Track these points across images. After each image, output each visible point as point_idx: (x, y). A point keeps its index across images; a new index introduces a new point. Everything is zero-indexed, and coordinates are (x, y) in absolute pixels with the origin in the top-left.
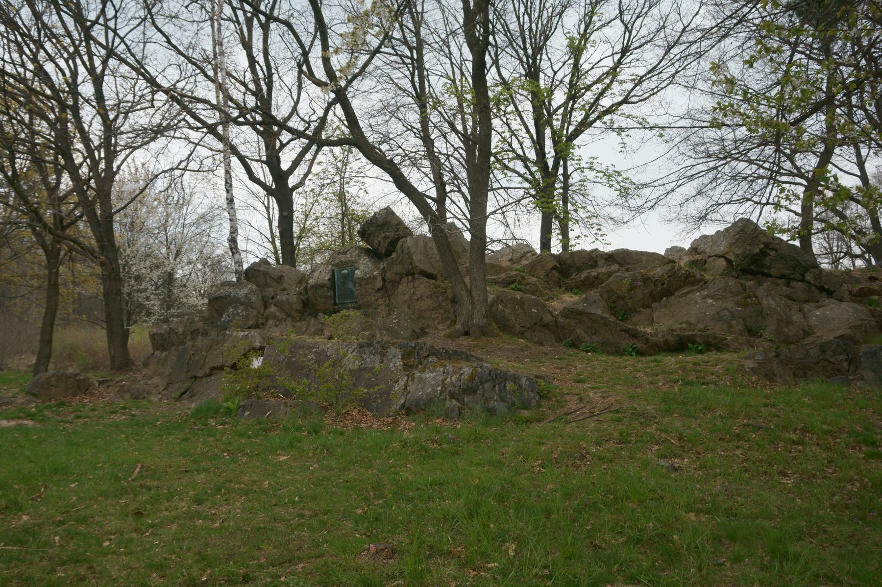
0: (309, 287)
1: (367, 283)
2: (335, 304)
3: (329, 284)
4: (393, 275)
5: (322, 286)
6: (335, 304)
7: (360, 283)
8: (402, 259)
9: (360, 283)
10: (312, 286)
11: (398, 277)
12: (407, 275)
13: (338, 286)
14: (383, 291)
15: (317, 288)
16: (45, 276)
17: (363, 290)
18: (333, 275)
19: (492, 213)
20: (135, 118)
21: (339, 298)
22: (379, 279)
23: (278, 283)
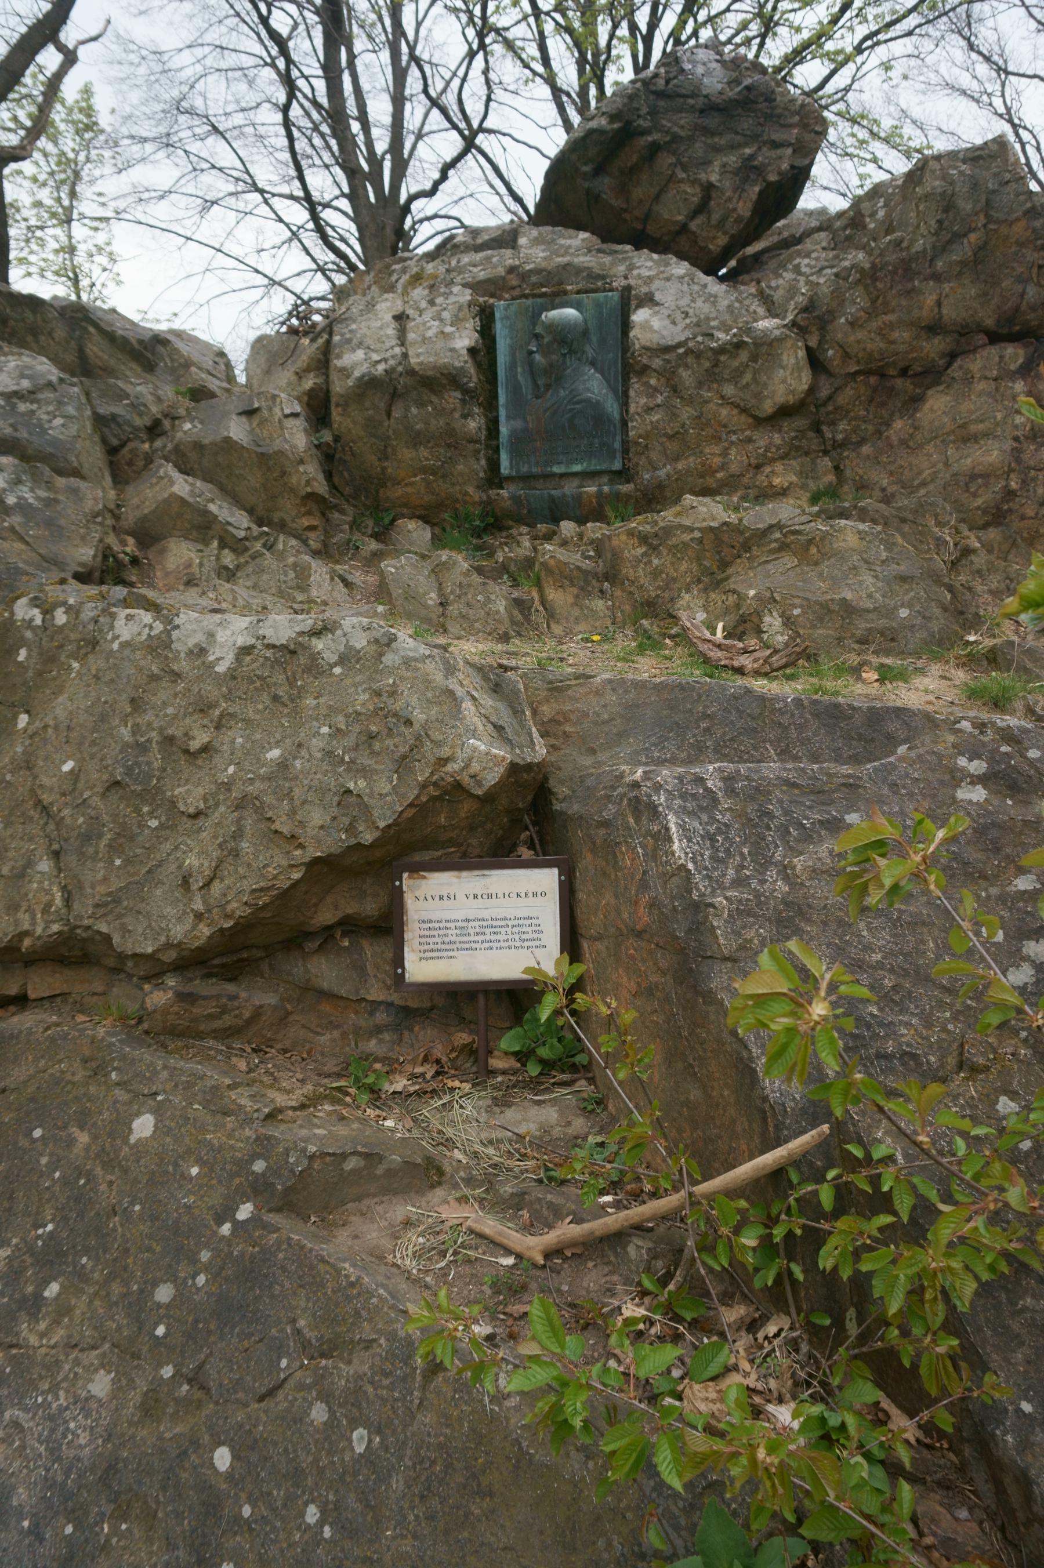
0: (339, 387)
1: (712, 377)
2: (494, 478)
3: (473, 378)
4: (902, 335)
5: (451, 379)
6: (494, 478)
7: (669, 376)
8: (981, 248)
9: (669, 376)
10: (370, 384)
11: (933, 347)
12: (994, 338)
13: (515, 389)
14: (801, 422)
15: (395, 395)
16: (758, 396)
17: (686, 413)
18: (486, 331)
19: (819, 201)
20: (434, 671)
21: (516, 452)
22: (794, 356)
23: (869, 1548)
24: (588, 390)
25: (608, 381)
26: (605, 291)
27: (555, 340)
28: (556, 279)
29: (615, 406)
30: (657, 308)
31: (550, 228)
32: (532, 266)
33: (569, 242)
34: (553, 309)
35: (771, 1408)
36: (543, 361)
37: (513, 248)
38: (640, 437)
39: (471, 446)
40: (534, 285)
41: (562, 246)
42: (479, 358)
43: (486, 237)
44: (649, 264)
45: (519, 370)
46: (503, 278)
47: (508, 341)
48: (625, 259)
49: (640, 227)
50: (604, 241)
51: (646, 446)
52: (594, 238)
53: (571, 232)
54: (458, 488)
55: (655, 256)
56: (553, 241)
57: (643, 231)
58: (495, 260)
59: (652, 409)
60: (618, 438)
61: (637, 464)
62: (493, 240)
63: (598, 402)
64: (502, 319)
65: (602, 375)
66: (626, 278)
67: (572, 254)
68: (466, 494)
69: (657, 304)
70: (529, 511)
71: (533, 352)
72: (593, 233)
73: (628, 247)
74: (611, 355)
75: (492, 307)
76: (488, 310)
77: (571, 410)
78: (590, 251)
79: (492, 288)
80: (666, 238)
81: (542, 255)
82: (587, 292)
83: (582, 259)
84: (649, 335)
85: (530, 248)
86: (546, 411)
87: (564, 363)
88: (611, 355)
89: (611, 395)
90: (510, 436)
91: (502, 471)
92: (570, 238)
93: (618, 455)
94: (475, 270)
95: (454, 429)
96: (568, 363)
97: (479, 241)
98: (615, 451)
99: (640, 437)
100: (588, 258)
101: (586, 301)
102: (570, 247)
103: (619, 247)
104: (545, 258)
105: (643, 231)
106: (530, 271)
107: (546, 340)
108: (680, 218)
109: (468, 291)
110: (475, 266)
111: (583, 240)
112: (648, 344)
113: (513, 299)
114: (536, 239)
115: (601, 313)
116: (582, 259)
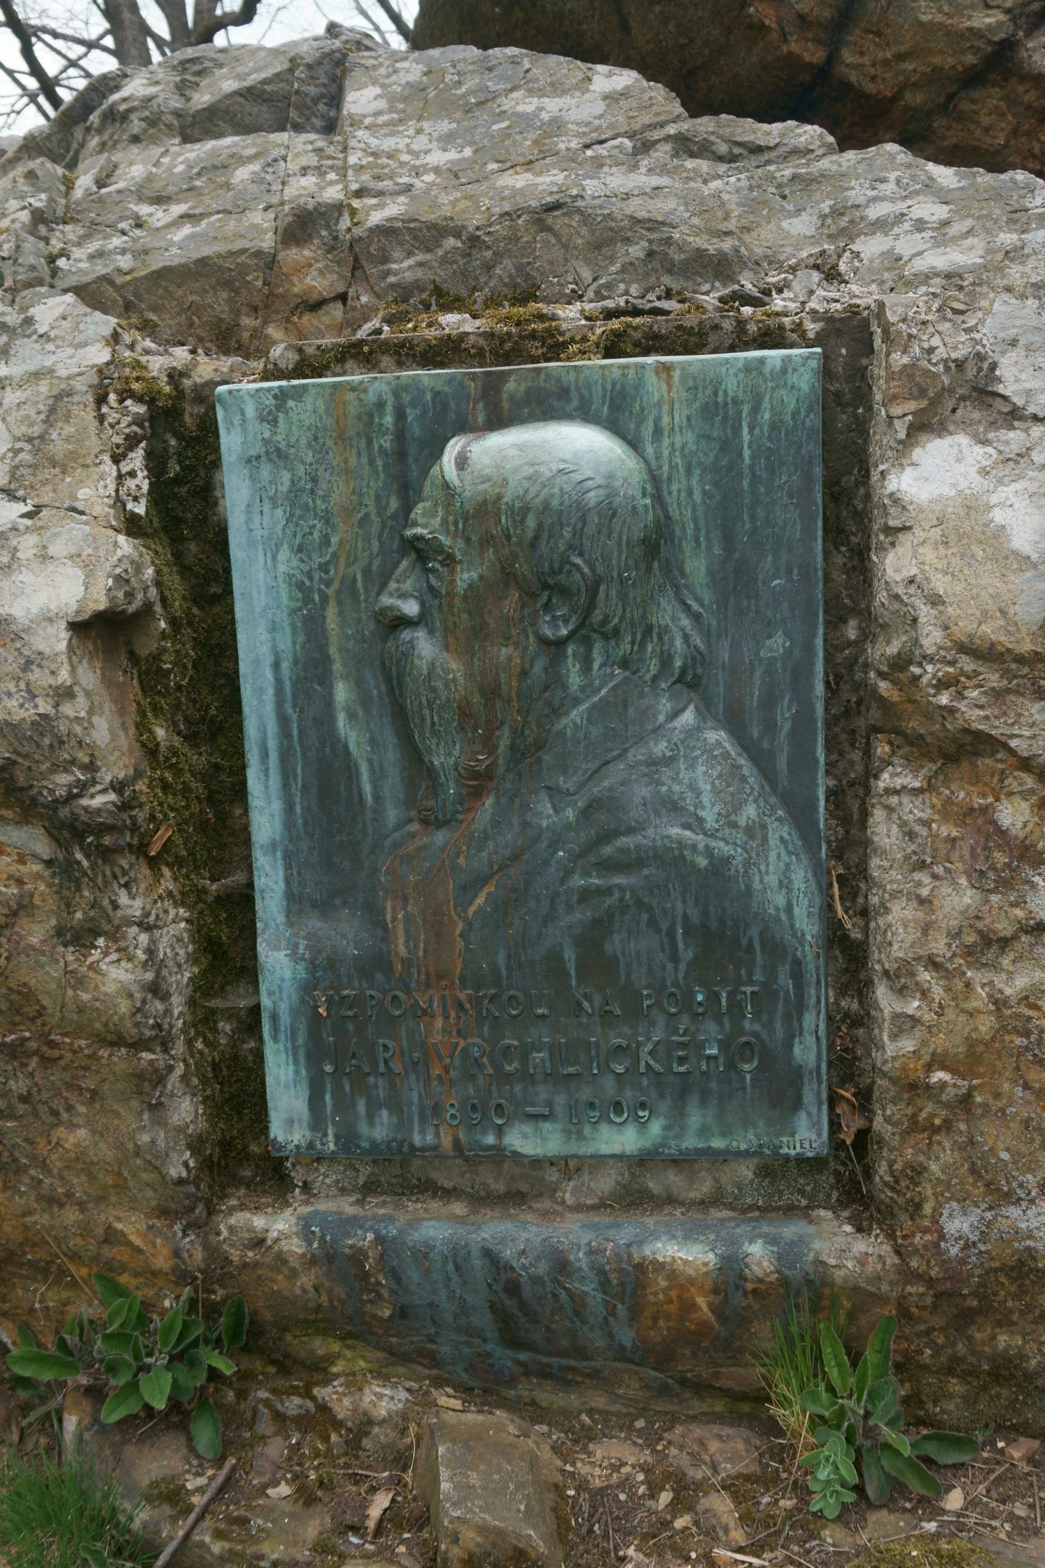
24: (673, 807)
25: (762, 761)
26: (741, 341)
27: (507, 576)
28: (504, 269)
29: (801, 877)
30: (1014, 438)
31: (472, 52)
32: (394, 209)
33: (552, 105)
34: (497, 422)
35: (516, 452)
36: (455, 667)
37: (330, 128)
38: (938, 1061)
39: (118, 1059)
40: (404, 292)
41: (524, 121)
42: (146, 647)
43: (229, 85)
44: (931, 210)
45: (342, 693)
46: (269, 262)
47: (286, 561)
48: (805, 183)
49: (814, 55)
50: (696, 107)
51: (965, 1101)
52: (658, 92)
53: (558, 64)
54: (71, 1216)
55: (945, 175)
56: (487, 99)
57: (824, 72)
58: (242, 174)
59: (1005, 943)
60: (814, 1021)
61: (917, 1172)
62: (249, 94)
63: (719, 865)
64: (252, 461)
65: (736, 728)
66: (832, 276)
67: (571, 159)
68: (111, 1237)
69: (1014, 415)
70: (402, 1313)
71: (401, 622)
72: (649, 72)
73: (809, 134)
74: (777, 644)
75: (204, 396)
76: (191, 413)
77: (586, 895)
78: (646, 147)
79: (220, 304)
80: (915, 98)
81: (438, 157)
82: (652, 344)
83: (617, 180)
84: (989, 581)
85: (392, 127)
86: (469, 888)
87: (555, 678)
88: (777, 644)
89: (779, 832)
90: (307, 988)
91: (277, 1131)
92: (557, 89)
93: (813, 1093)
94: (158, 216)
95: (28, 994)
96: (575, 679)
97: (202, 99)
98: (796, 1076)
99: (938, 1061)
100: (641, 179)
101: (654, 388)
102: (557, 126)
103: (771, 132)
104: (454, 172)
105: (824, 72)
106: (386, 231)
107: (465, 577)
108: (985, 20)
109: (105, 323)
110: (159, 200)
111: (611, 98)
112: (990, 631)
113: (306, 367)
114: (416, 90)
115: (729, 446)
116: (617, 180)
